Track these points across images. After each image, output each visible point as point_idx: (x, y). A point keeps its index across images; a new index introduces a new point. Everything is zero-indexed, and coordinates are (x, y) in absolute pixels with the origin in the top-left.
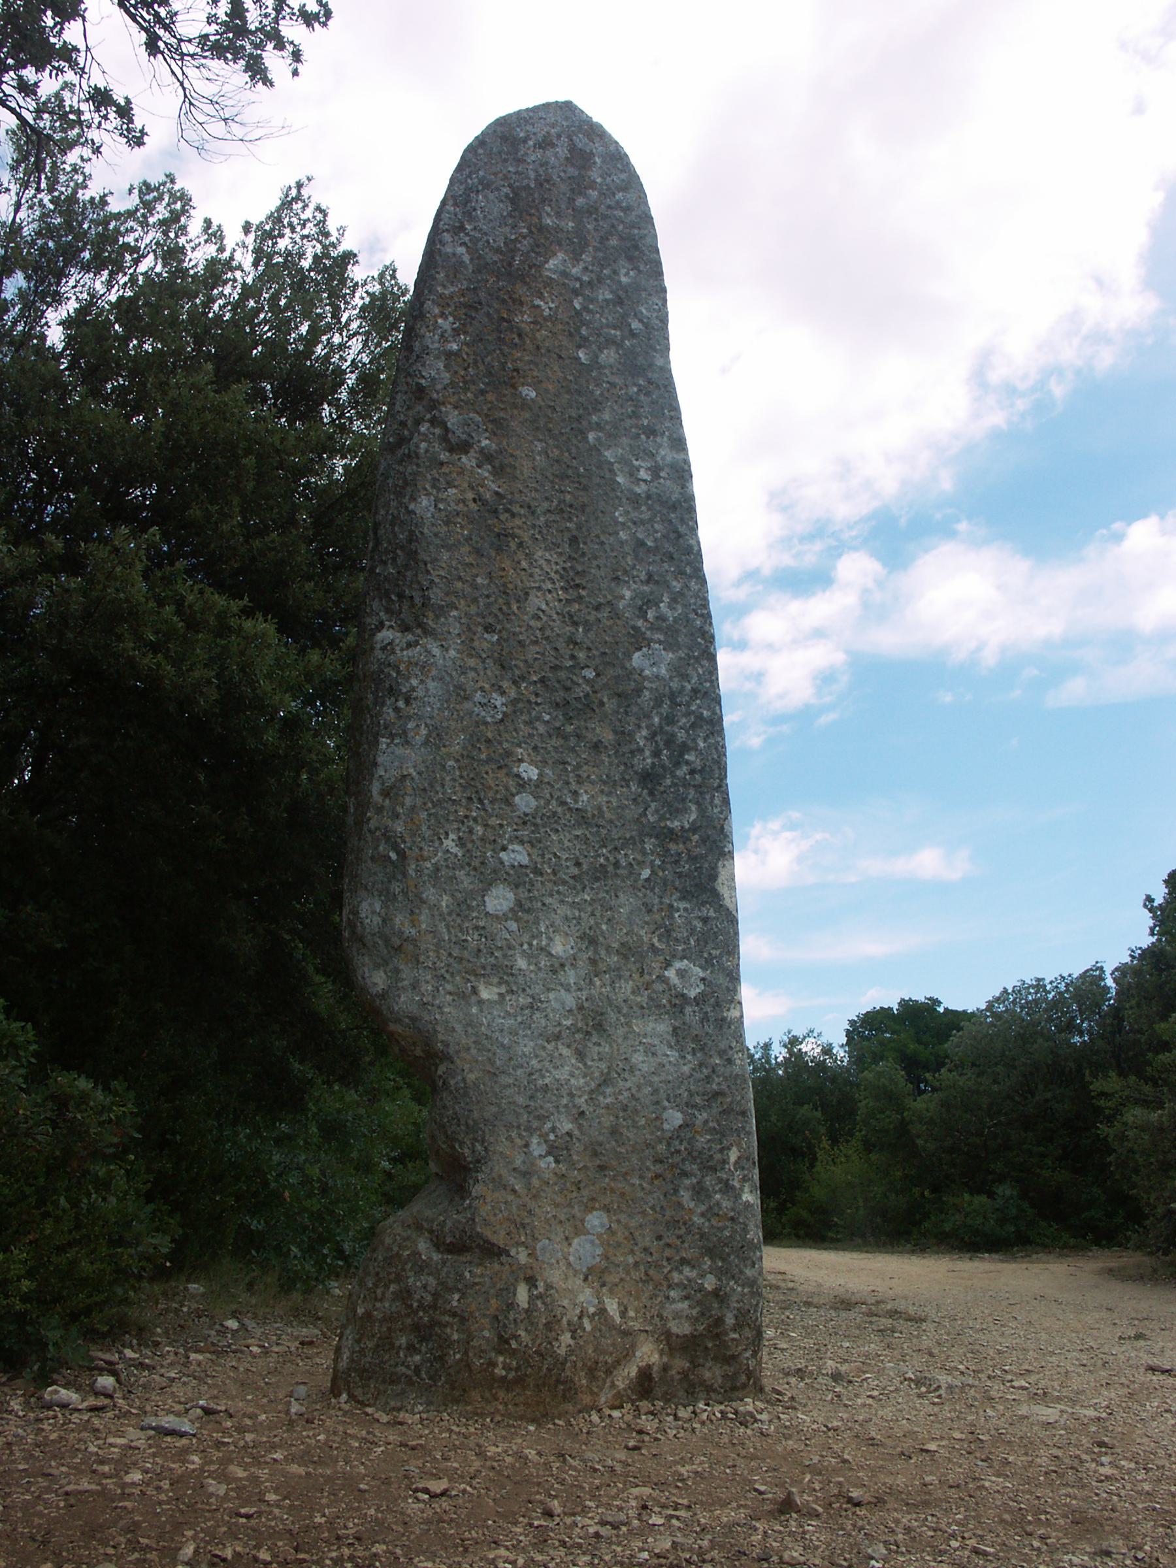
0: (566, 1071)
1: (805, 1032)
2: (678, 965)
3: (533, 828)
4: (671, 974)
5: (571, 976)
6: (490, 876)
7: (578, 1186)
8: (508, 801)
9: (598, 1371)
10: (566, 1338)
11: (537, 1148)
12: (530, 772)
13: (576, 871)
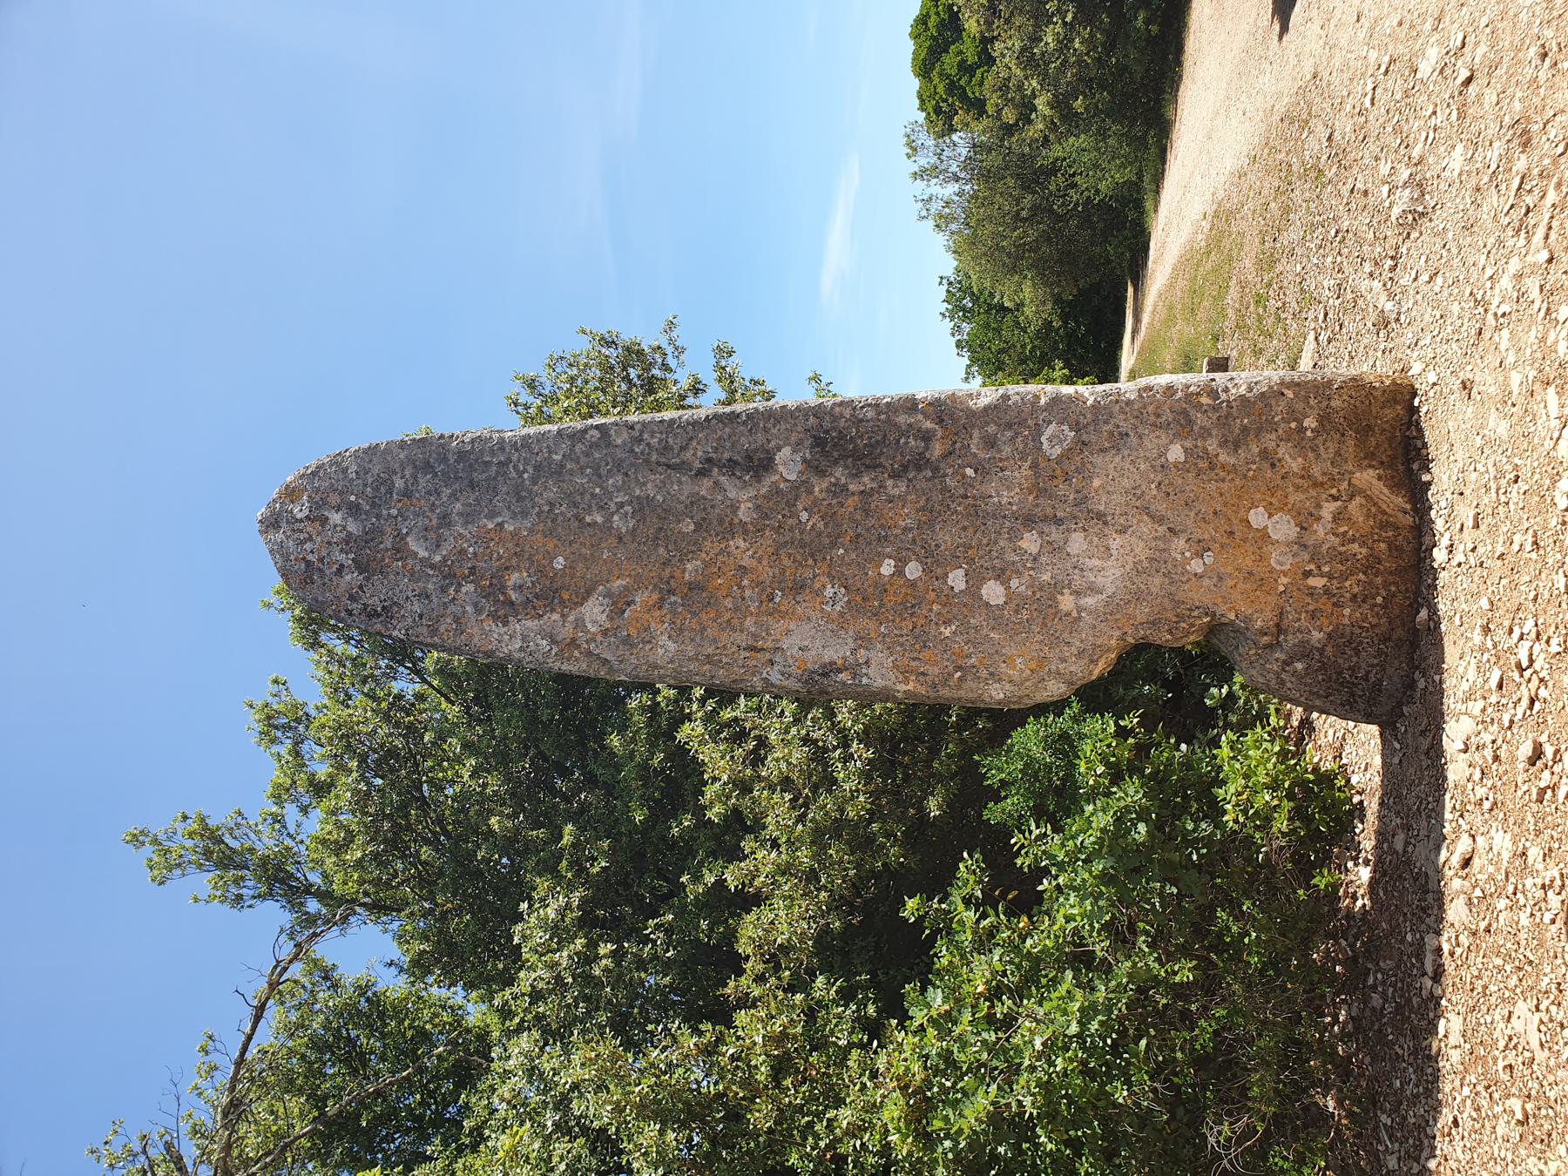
2: (1046, 445)
8: (913, 584)
12: (887, 568)
13: (971, 530)
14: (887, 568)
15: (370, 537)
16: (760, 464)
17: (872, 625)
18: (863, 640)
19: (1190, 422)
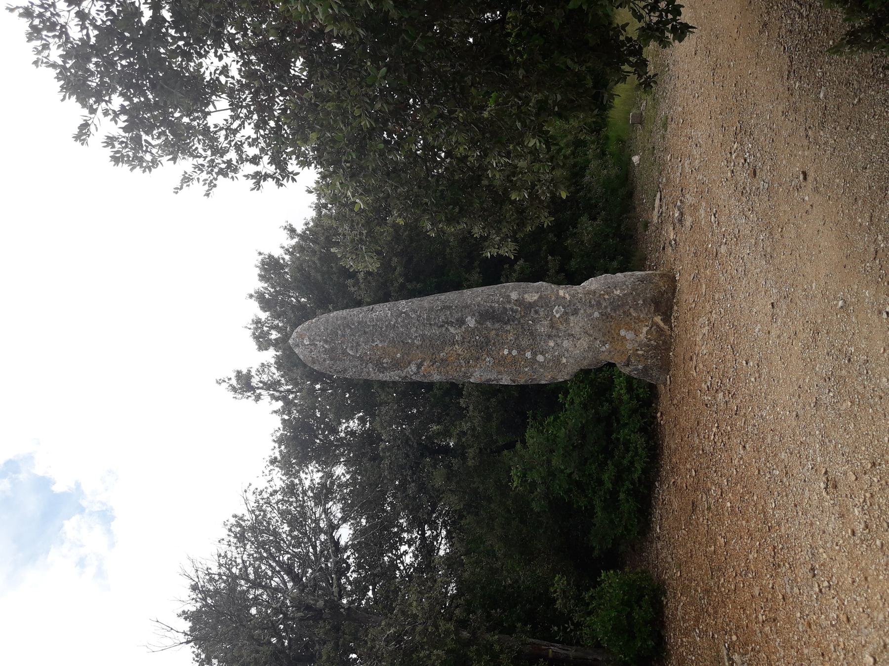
0: (584, 343)
1: (43, 68)
3: (522, 351)
4: (557, 316)
5: (559, 341)
6: (534, 360)
7: (613, 338)
9: (660, 330)
10: (652, 342)
11: (604, 349)
14: (506, 352)
15: (333, 350)
16: (461, 322)
17: (502, 369)
18: (499, 373)
19: (601, 304)
